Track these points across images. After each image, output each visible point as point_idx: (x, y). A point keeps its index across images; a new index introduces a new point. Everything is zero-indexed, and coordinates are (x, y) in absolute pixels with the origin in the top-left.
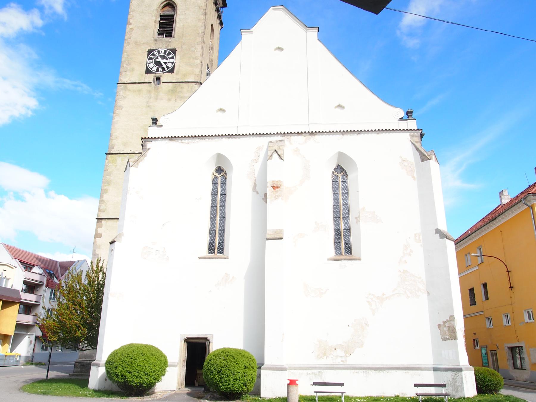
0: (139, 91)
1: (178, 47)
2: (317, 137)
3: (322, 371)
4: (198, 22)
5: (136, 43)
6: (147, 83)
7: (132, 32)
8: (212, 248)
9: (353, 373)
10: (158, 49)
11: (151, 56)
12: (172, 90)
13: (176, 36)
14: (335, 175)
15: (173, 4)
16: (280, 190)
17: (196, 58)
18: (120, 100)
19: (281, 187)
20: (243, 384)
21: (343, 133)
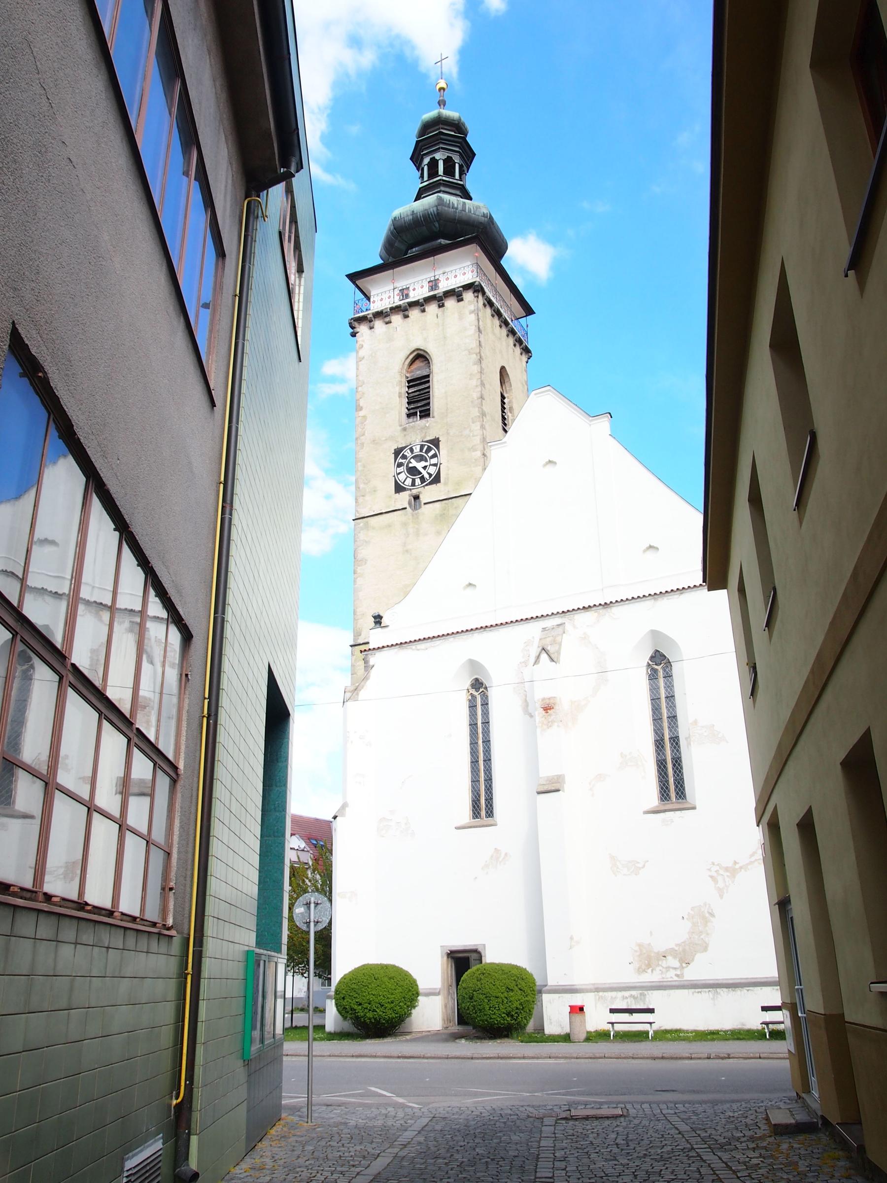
0: (389, 526)
1: (441, 434)
2: (616, 610)
3: (646, 992)
4: (470, 379)
5: (374, 441)
6: (399, 510)
7: (365, 423)
8: (476, 810)
9: (693, 993)
10: (410, 445)
11: (401, 461)
12: (441, 515)
13: (435, 414)
14: (653, 669)
15: (425, 354)
16: (554, 712)
17: (473, 449)
18: (360, 548)
19: (556, 707)
20: (507, 1015)
21: (656, 596)
